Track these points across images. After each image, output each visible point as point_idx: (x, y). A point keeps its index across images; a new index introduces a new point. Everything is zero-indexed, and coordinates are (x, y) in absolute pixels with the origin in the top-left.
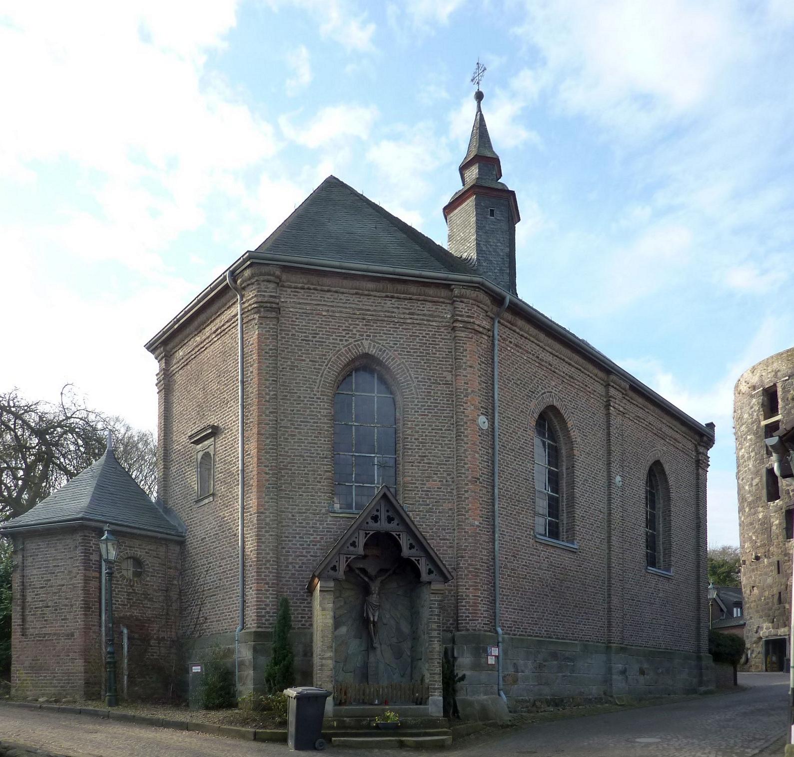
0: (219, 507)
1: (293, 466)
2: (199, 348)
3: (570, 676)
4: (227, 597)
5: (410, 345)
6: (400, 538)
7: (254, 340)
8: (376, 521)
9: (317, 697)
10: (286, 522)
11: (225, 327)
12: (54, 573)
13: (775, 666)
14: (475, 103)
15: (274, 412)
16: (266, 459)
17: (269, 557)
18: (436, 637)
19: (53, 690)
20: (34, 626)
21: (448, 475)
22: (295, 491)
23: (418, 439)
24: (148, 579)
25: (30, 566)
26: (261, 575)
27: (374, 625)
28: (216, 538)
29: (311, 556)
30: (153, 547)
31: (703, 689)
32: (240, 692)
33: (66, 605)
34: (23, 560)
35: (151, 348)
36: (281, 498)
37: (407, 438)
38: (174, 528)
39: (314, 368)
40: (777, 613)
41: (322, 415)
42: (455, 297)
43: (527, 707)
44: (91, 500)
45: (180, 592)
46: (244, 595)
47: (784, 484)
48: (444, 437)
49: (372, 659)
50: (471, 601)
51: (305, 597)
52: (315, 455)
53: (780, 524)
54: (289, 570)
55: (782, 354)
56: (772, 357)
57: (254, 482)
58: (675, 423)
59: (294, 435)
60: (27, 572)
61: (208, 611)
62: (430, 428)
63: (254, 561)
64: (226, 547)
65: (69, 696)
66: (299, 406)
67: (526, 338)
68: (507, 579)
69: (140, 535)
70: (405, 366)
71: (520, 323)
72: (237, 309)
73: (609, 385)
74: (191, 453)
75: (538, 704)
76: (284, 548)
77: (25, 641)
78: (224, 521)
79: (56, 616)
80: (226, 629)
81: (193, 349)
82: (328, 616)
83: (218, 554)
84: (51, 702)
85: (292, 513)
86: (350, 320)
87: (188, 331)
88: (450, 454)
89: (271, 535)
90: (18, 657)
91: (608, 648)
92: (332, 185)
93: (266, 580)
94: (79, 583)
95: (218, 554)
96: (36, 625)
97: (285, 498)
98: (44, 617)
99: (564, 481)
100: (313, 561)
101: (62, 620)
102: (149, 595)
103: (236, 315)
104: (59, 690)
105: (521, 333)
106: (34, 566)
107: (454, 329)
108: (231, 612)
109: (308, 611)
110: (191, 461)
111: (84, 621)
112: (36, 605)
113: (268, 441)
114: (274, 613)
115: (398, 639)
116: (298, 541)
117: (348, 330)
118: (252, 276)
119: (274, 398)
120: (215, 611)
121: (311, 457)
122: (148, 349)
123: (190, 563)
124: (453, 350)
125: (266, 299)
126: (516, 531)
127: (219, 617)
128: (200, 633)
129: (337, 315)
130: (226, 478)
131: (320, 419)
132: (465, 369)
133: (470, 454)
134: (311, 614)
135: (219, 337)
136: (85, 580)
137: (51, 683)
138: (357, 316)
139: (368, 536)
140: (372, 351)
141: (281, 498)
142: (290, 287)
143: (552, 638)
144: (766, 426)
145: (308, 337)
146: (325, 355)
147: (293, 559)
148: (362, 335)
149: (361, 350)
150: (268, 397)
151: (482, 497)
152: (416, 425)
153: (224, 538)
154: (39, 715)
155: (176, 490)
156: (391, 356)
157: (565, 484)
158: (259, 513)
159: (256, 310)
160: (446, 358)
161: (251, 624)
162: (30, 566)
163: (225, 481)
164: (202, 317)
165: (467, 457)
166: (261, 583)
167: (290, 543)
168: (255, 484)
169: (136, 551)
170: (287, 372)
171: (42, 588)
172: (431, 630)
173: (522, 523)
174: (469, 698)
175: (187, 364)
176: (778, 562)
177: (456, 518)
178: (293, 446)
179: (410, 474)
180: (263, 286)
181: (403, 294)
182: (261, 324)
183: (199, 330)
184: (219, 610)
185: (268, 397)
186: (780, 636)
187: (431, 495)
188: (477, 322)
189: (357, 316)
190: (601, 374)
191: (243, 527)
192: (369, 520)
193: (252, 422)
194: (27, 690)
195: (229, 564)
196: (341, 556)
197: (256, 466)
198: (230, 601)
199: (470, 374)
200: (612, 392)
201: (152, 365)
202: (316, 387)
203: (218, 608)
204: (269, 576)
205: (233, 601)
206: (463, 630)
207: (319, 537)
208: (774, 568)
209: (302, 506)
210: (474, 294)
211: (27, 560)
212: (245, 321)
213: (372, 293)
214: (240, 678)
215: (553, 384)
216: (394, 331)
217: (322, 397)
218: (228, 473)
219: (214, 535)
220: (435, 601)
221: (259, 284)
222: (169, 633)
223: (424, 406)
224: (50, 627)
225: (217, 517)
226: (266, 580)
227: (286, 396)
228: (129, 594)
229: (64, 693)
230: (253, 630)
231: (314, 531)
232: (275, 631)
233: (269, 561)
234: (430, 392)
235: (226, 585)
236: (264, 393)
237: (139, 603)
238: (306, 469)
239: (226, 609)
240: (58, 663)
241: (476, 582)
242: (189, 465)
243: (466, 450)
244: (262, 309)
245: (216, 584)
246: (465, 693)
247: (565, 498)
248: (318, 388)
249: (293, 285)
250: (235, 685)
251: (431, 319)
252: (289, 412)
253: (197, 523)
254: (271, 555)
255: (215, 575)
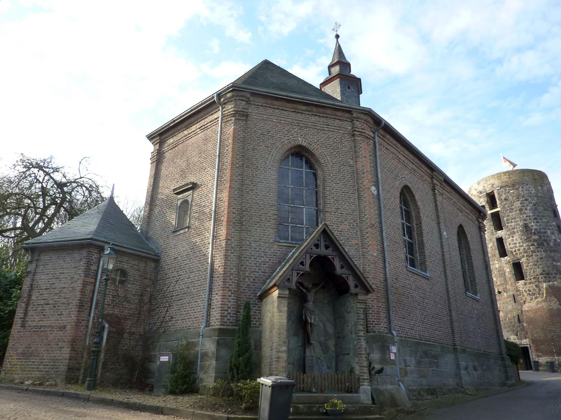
0: (192, 235)
1: (252, 210)
2: (186, 137)
3: (436, 370)
4: (193, 301)
5: (327, 143)
6: (334, 260)
7: (230, 132)
8: (318, 248)
9: (282, 386)
10: (245, 247)
11: (208, 125)
12: (59, 278)
13: (523, 366)
14: (335, 40)
15: (242, 175)
16: (234, 204)
17: (232, 271)
18: (362, 336)
19: (38, 374)
20: (34, 319)
21: (354, 221)
22: (252, 226)
23: (334, 198)
24: (129, 286)
25: (40, 273)
26: (226, 285)
27: (311, 326)
28: (187, 257)
29: (262, 272)
30: (136, 263)
31: (509, 382)
32: (202, 380)
33: (64, 304)
34: (36, 268)
35: (151, 138)
36: (242, 230)
37: (327, 197)
38: (152, 250)
39: (268, 151)
40: (519, 329)
41: (271, 179)
42: (354, 118)
43: (415, 396)
44: (97, 227)
45: (151, 297)
46: (210, 299)
47: (509, 248)
48: (350, 198)
49: (308, 353)
50: (376, 310)
51: (257, 303)
52: (266, 203)
53: (510, 271)
54: (246, 282)
55: (494, 175)
56: (489, 177)
57: (224, 219)
58: (466, 203)
59: (253, 190)
60: (37, 277)
61: (174, 312)
62: (341, 192)
63: (221, 274)
64: (196, 264)
65: (51, 380)
66: (257, 172)
67: (390, 145)
68: (393, 295)
69: (130, 254)
70: (324, 153)
71: (388, 136)
72: (219, 114)
73: (433, 177)
74: (172, 201)
75: (422, 393)
76: (242, 265)
77: (23, 332)
78: (196, 245)
79: (54, 312)
80: (189, 326)
81: (182, 138)
82: (284, 317)
83: (188, 269)
84: (35, 385)
85: (249, 241)
86: (290, 125)
87: (179, 127)
88: (355, 208)
89: (235, 256)
90: (14, 345)
91: (455, 349)
92: (266, 65)
93: (229, 288)
94: (78, 287)
95: (188, 269)
96: (35, 318)
97: (245, 230)
98: (43, 312)
99: (415, 233)
100: (263, 276)
101: (58, 315)
102: (128, 298)
103: (218, 118)
104: (44, 374)
105: (388, 142)
106: (44, 272)
107: (353, 135)
108: (195, 312)
109: (259, 313)
110: (171, 205)
111: (77, 317)
112: (38, 302)
113: (236, 192)
114: (234, 314)
115: (324, 337)
116: (253, 261)
117: (289, 131)
118: (232, 97)
119: (242, 166)
120: (181, 312)
121: (264, 204)
122: (148, 138)
123: (162, 275)
124: (353, 147)
125: (240, 110)
126: (396, 262)
127: (184, 317)
128: (165, 329)
129: (283, 122)
130: (200, 216)
131: (271, 181)
132: (362, 158)
133: (368, 209)
134: (261, 316)
135: (203, 130)
136: (84, 284)
137: (38, 368)
138: (294, 124)
139: (312, 258)
140: (304, 144)
141: (242, 230)
142: (254, 105)
143: (422, 340)
144: (492, 214)
145: (264, 133)
146: (275, 144)
147: (249, 274)
148: (298, 135)
149: (296, 143)
150: (238, 165)
151: (377, 237)
152: (332, 189)
153: (195, 257)
154: (27, 397)
155: (157, 224)
156: (315, 148)
157: (416, 234)
158: (227, 240)
159: (234, 115)
160: (349, 151)
161: (215, 322)
162: (40, 273)
163: (198, 218)
164: (192, 120)
165: (366, 211)
166: (226, 290)
167: (247, 262)
168: (225, 220)
169: (123, 265)
170: (250, 151)
171: (47, 289)
172: (359, 330)
173: (399, 257)
174: (379, 387)
175: (175, 147)
176: (513, 295)
177: (360, 250)
178: (252, 197)
179: (329, 219)
180: (238, 102)
181: (323, 114)
182: (236, 123)
183: (187, 127)
184: (185, 311)
185: (238, 165)
186: (524, 345)
187: (344, 234)
188: (367, 133)
189: (294, 124)
190: (428, 171)
191: (213, 249)
192: (313, 247)
193: (226, 180)
194: (15, 374)
195: (197, 276)
196: (294, 272)
197: (227, 208)
198: (195, 304)
199: (365, 161)
200: (435, 181)
201: (150, 148)
202: (268, 162)
203: (184, 309)
204: (232, 285)
205: (199, 304)
206: (371, 332)
207: (267, 259)
208: (511, 299)
209: (257, 237)
210: (365, 117)
211: (38, 268)
212: (224, 121)
213: (304, 112)
214: (202, 368)
215: (406, 173)
216: (317, 134)
217: (272, 168)
218: (202, 213)
219: (186, 255)
220: (360, 308)
221: (235, 101)
222: (138, 329)
223: (337, 178)
224: (47, 320)
225: (190, 243)
226: (229, 288)
227: (249, 166)
228: (114, 296)
229: (48, 377)
230: (218, 327)
231: (264, 255)
232: (239, 329)
233: (232, 274)
234: (340, 170)
235: (192, 292)
236: (235, 162)
237: (120, 304)
238: (260, 212)
239: (191, 310)
240: (48, 350)
241: (378, 296)
242: (169, 208)
243: (365, 206)
244: (237, 115)
245: (184, 291)
246: (376, 383)
247: (417, 243)
248: (270, 162)
249: (256, 104)
250: (196, 373)
251: (340, 129)
252: (250, 175)
253: (172, 247)
254: (234, 270)
255: (183, 284)
